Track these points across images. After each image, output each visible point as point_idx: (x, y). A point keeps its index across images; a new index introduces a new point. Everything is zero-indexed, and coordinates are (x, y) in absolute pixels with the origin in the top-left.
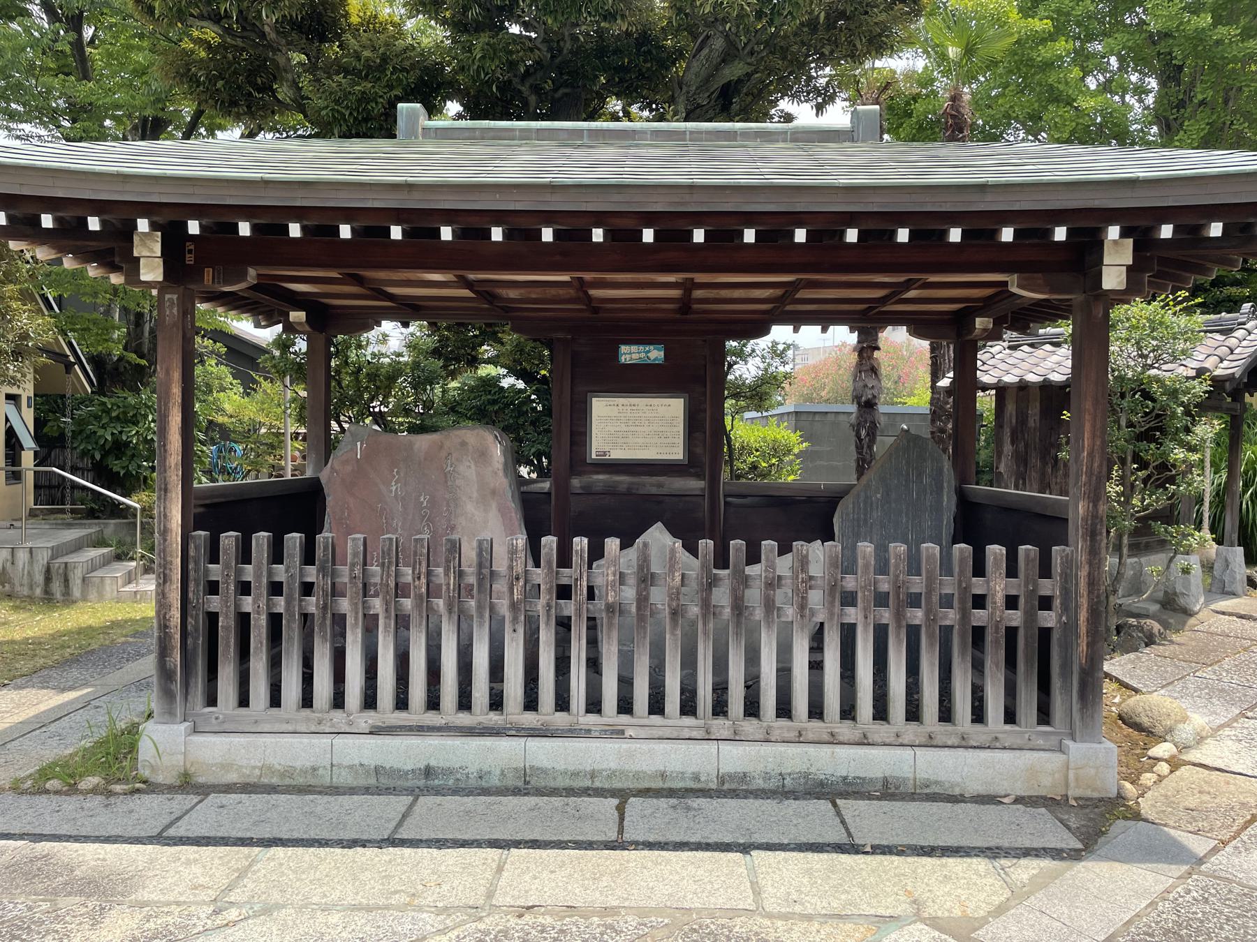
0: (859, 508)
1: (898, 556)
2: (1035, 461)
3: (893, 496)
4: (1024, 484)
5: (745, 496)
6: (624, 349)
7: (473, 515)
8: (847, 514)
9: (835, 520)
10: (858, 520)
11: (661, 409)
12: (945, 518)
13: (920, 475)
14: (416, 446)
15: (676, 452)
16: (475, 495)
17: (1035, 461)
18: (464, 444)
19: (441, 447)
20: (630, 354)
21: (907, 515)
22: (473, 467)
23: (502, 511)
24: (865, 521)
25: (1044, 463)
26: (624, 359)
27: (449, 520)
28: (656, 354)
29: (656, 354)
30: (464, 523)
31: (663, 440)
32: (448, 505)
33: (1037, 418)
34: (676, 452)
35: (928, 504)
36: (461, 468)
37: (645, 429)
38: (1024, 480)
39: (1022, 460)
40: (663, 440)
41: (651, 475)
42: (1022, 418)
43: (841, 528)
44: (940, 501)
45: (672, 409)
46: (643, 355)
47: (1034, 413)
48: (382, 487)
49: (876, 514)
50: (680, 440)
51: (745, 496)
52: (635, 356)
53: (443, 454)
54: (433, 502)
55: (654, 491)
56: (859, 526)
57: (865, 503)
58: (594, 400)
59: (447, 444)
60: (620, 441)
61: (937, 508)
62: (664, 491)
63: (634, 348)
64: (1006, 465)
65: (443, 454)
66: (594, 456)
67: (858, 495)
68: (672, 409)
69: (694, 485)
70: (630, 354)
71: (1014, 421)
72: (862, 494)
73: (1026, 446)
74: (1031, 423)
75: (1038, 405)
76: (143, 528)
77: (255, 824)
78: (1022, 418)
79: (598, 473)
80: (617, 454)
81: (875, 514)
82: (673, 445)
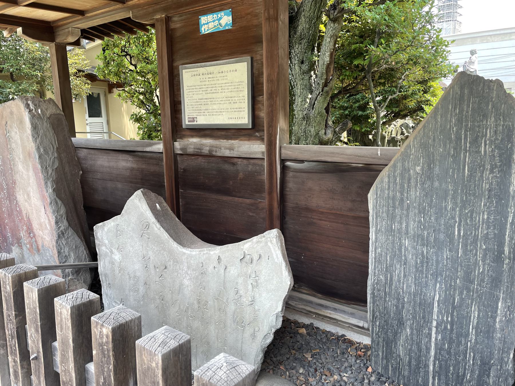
1: (180, 144)
3: (437, 170)
5: (302, 161)
6: (203, 19)
9: (369, 195)
13: (475, 142)
15: (242, 118)
21: (454, 198)
24: (402, 200)
34: (242, 118)
35: (486, 186)
41: (227, 138)
43: (375, 207)
51: (302, 161)
52: (211, 25)
55: (227, 153)
56: (394, 207)
57: (402, 176)
62: (234, 154)
66: (187, 123)
67: (395, 166)
69: (256, 148)
72: (399, 165)
76: (449, 4)
77: (106, 294)
79: (192, 136)
80: (202, 121)
81: (412, 193)
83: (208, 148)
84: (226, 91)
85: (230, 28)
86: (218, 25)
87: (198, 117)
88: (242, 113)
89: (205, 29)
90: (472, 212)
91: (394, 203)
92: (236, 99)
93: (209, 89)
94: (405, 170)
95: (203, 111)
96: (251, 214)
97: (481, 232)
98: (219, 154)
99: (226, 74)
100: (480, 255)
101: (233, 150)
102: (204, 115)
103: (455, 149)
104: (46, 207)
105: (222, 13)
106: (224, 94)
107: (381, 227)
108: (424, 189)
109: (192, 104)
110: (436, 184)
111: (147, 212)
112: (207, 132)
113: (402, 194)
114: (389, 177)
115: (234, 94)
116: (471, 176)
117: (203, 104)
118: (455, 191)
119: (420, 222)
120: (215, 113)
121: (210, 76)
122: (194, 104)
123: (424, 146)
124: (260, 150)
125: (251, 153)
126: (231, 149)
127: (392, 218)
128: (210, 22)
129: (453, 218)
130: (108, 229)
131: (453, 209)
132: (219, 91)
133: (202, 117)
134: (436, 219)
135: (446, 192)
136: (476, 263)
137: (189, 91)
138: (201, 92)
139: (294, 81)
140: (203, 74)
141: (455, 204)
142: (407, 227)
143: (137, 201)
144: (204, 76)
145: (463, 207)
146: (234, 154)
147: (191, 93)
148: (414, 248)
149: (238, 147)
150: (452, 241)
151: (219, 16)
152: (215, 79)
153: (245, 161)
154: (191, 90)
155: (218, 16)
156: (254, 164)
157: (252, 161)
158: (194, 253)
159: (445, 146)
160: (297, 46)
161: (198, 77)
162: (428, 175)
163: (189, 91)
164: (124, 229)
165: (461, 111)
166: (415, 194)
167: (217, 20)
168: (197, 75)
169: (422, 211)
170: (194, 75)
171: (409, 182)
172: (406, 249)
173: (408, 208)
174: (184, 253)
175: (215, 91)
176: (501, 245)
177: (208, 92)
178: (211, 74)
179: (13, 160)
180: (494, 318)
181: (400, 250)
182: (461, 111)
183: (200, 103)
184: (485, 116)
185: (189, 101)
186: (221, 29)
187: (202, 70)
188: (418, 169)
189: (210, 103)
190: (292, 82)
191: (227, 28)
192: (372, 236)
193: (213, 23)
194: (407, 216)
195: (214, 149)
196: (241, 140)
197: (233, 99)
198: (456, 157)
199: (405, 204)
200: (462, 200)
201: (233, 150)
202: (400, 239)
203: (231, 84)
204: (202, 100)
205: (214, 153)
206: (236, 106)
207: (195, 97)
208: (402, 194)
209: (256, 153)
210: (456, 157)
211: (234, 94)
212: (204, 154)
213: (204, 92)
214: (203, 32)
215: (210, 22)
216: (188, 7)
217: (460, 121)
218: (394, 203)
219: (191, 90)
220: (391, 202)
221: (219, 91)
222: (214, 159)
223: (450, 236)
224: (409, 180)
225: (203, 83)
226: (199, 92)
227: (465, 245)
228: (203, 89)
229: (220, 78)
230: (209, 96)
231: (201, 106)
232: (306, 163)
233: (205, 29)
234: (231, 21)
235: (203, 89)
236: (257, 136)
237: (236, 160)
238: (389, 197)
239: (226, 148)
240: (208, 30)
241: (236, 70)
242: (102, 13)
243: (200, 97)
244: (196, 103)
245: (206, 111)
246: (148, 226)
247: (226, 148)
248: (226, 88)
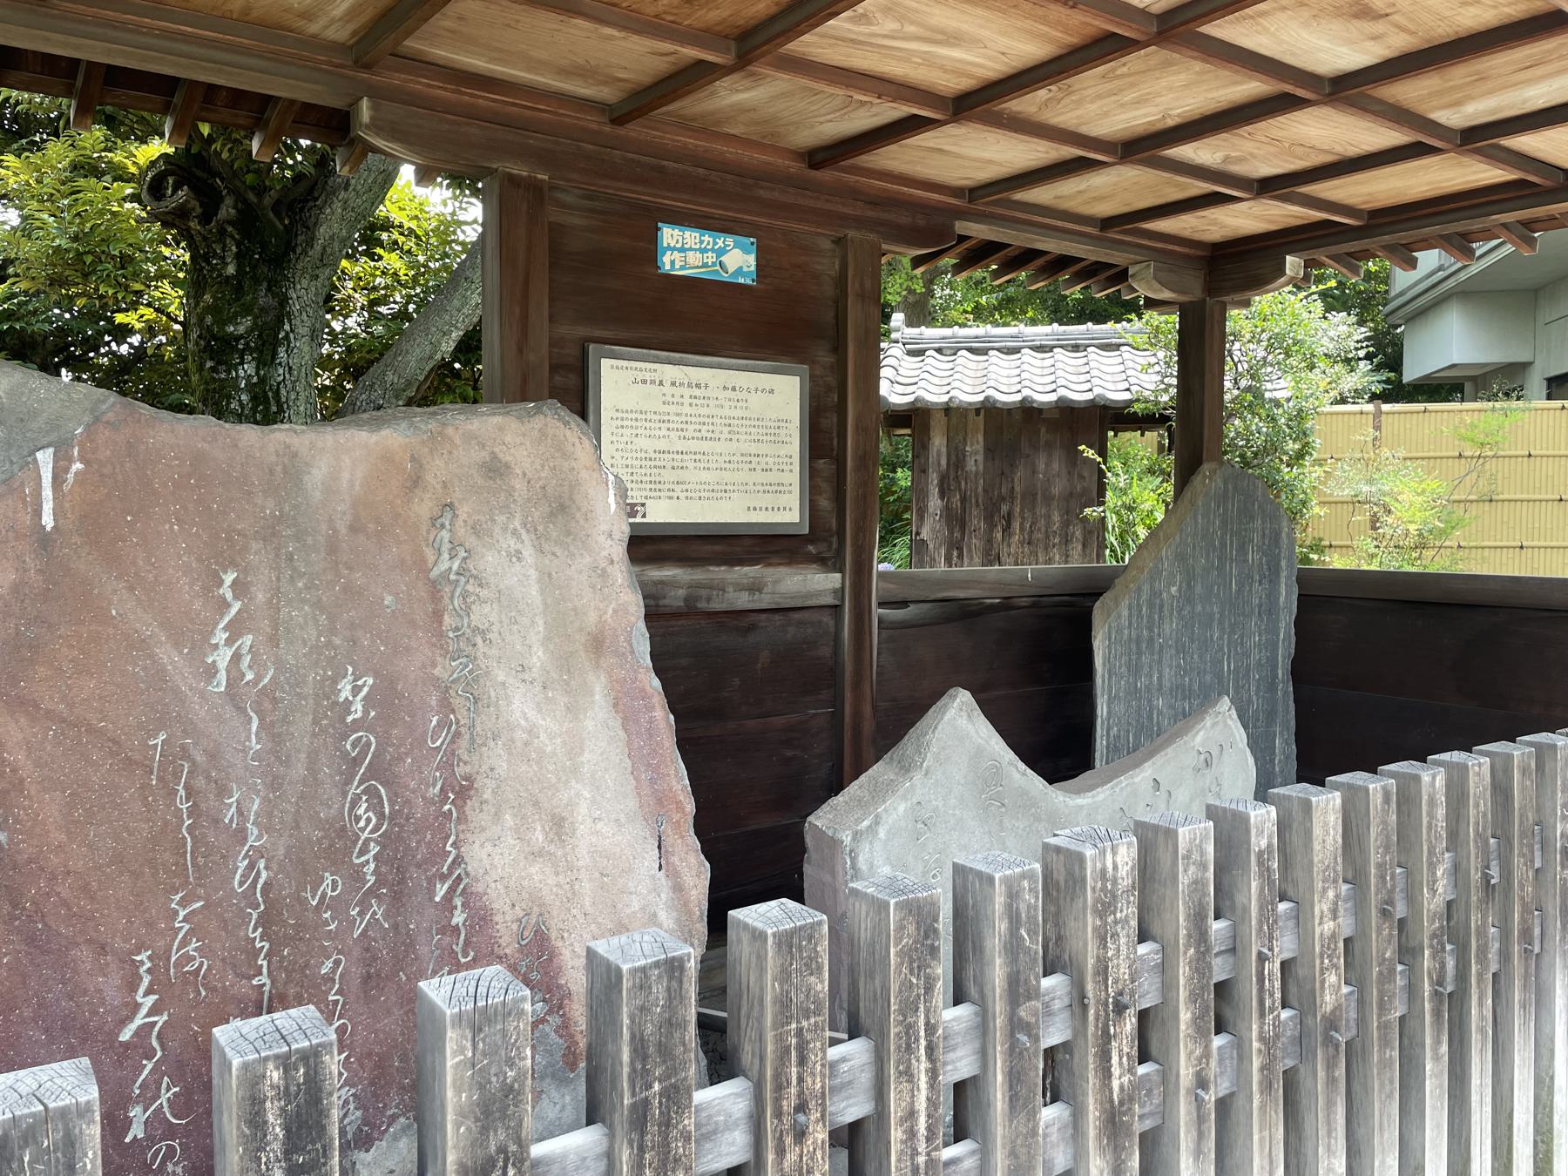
0: (1140, 615)
2: (977, 521)
3: (1199, 589)
4: (960, 556)
5: (904, 604)
6: (669, 235)
7: (532, 731)
8: (1119, 630)
10: (1138, 642)
11: (755, 400)
12: (1282, 625)
13: (1242, 549)
14: (317, 475)
15: (785, 508)
16: (538, 657)
17: (977, 521)
18: (495, 469)
19: (415, 482)
20: (685, 251)
22: (528, 553)
23: (625, 705)
24: (1151, 640)
25: (992, 526)
26: (671, 263)
27: (448, 765)
28: (737, 260)
29: (737, 260)
30: (502, 768)
31: (760, 477)
32: (446, 706)
33: (980, 458)
34: (785, 508)
35: (1256, 601)
36: (489, 561)
37: (718, 447)
38: (960, 549)
39: (956, 520)
40: (760, 477)
42: (957, 459)
43: (1107, 660)
44: (1273, 595)
45: (772, 399)
46: (710, 258)
47: (975, 449)
48: (169, 656)
49: (1170, 627)
50: (792, 476)
52: (694, 258)
53: (423, 507)
54: (386, 699)
55: (743, 601)
56: (1139, 653)
57: (1151, 605)
58: (606, 363)
59: (437, 470)
60: (668, 475)
61: (1270, 609)
62: (765, 601)
63: (691, 237)
64: (933, 530)
65: (423, 507)
68: (772, 399)
69: (816, 583)
70: (685, 251)
71: (944, 462)
72: (1146, 587)
73: (963, 500)
74: (971, 466)
75: (981, 438)
78: (957, 459)
82: (778, 489)
83: (681, 592)
84: (743, 437)
85: (749, 282)
86: (714, 264)
87: (648, 502)
88: (786, 496)
89: (673, 262)
90: (1242, 636)
91: (1139, 647)
92: (770, 460)
93: (691, 428)
94: (1155, 594)
95: (667, 486)
96: (789, 754)
97: (1255, 656)
98: (717, 606)
99: (744, 395)
100: (1253, 688)
101: (760, 591)
102: (670, 498)
103: (1220, 559)
104: (670, 839)
105: (730, 240)
106: (735, 444)
107: (1118, 690)
108: (1181, 617)
109: (629, 462)
110: (1199, 608)
111: (993, 742)
112: (665, 547)
113: (1151, 630)
114: (1130, 609)
115: (763, 449)
116: (1239, 591)
117: (669, 465)
118: (1222, 614)
119: (1179, 666)
120: (706, 494)
121: (697, 392)
122: (638, 463)
123: (1181, 557)
124: (830, 586)
125: (809, 595)
126: (755, 588)
127: (1135, 670)
128: (691, 249)
129: (1221, 649)
130: (889, 832)
131: (1221, 638)
132: (723, 437)
133: (664, 503)
134: (1200, 657)
135: (1211, 616)
136: (1250, 701)
137: (619, 423)
138: (664, 432)
139: (290, 386)
140: (673, 384)
141: (1222, 630)
142: (1160, 678)
143: (963, 722)
144: (678, 391)
145: (1233, 632)
146: (761, 601)
147: (627, 432)
148: (1171, 707)
149: (776, 582)
150: (1220, 681)
151: (720, 243)
152: (711, 402)
153: (777, 617)
154: (628, 423)
155: (715, 243)
156: (801, 623)
157: (797, 616)
158: (1101, 797)
159: (1208, 555)
160: (305, 283)
161: (655, 388)
162: (1187, 597)
163: (619, 423)
164: (936, 809)
165: (1226, 510)
166: (1170, 627)
167: (712, 250)
168: (652, 382)
169: (1181, 649)
170: (644, 382)
171: (1161, 611)
172: (1160, 713)
173: (1161, 650)
174: (1081, 807)
175: (709, 435)
176: (1274, 668)
177: (687, 434)
178: (698, 386)
179: (473, 682)
180: (1272, 761)
181: (1150, 718)
182: (1226, 510)
183: (658, 463)
184: (1252, 518)
185: (618, 455)
186: (725, 277)
187: (670, 372)
188: (1174, 589)
189: (691, 465)
190: (283, 392)
191: (741, 281)
192: (1102, 709)
193: (699, 255)
194: (1160, 662)
195: (704, 593)
196: (770, 565)
197: (764, 460)
198: (1221, 569)
199: (1157, 646)
200: (1230, 625)
201: (760, 591)
202: (1150, 701)
203: (639, 416)
204: (666, 456)
205: (702, 605)
206: (772, 477)
207: (642, 443)
208: (1151, 630)
209: (820, 593)
210: (1221, 569)
211: (763, 449)
212: (667, 610)
213: (673, 434)
214: (668, 267)
215: (691, 249)
216: (639, 189)
217: (1224, 523)
218: (1139, 647)
219: (628, 423)
220: (1134, 646)
221: (723, 437)
222: (684, 622)
223: (1219, 676)
224: (1162, 606)
225: (672, 409)
226: (657, 433)
227: (1236, 681)
228: (671, 426)
229: (727, 404)
230: (694, 445)
231: (662, 471)
232: (912, 607)
233: (673, 262)
234: (753, 268)
235: (671, 426)
236: (810, 553)
237: (753, 618)
238: (1130, 639)
239: (740, 588)
240: (682, 268)
241: (772, 391)
242: (187, 38)
243: (662, 445)
244: (644, 463)
245: (678, 488)
246: (997, 772)
247: (740, 588)
248: (743, 430)
